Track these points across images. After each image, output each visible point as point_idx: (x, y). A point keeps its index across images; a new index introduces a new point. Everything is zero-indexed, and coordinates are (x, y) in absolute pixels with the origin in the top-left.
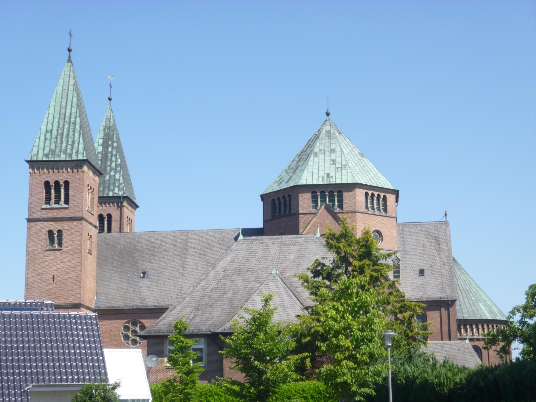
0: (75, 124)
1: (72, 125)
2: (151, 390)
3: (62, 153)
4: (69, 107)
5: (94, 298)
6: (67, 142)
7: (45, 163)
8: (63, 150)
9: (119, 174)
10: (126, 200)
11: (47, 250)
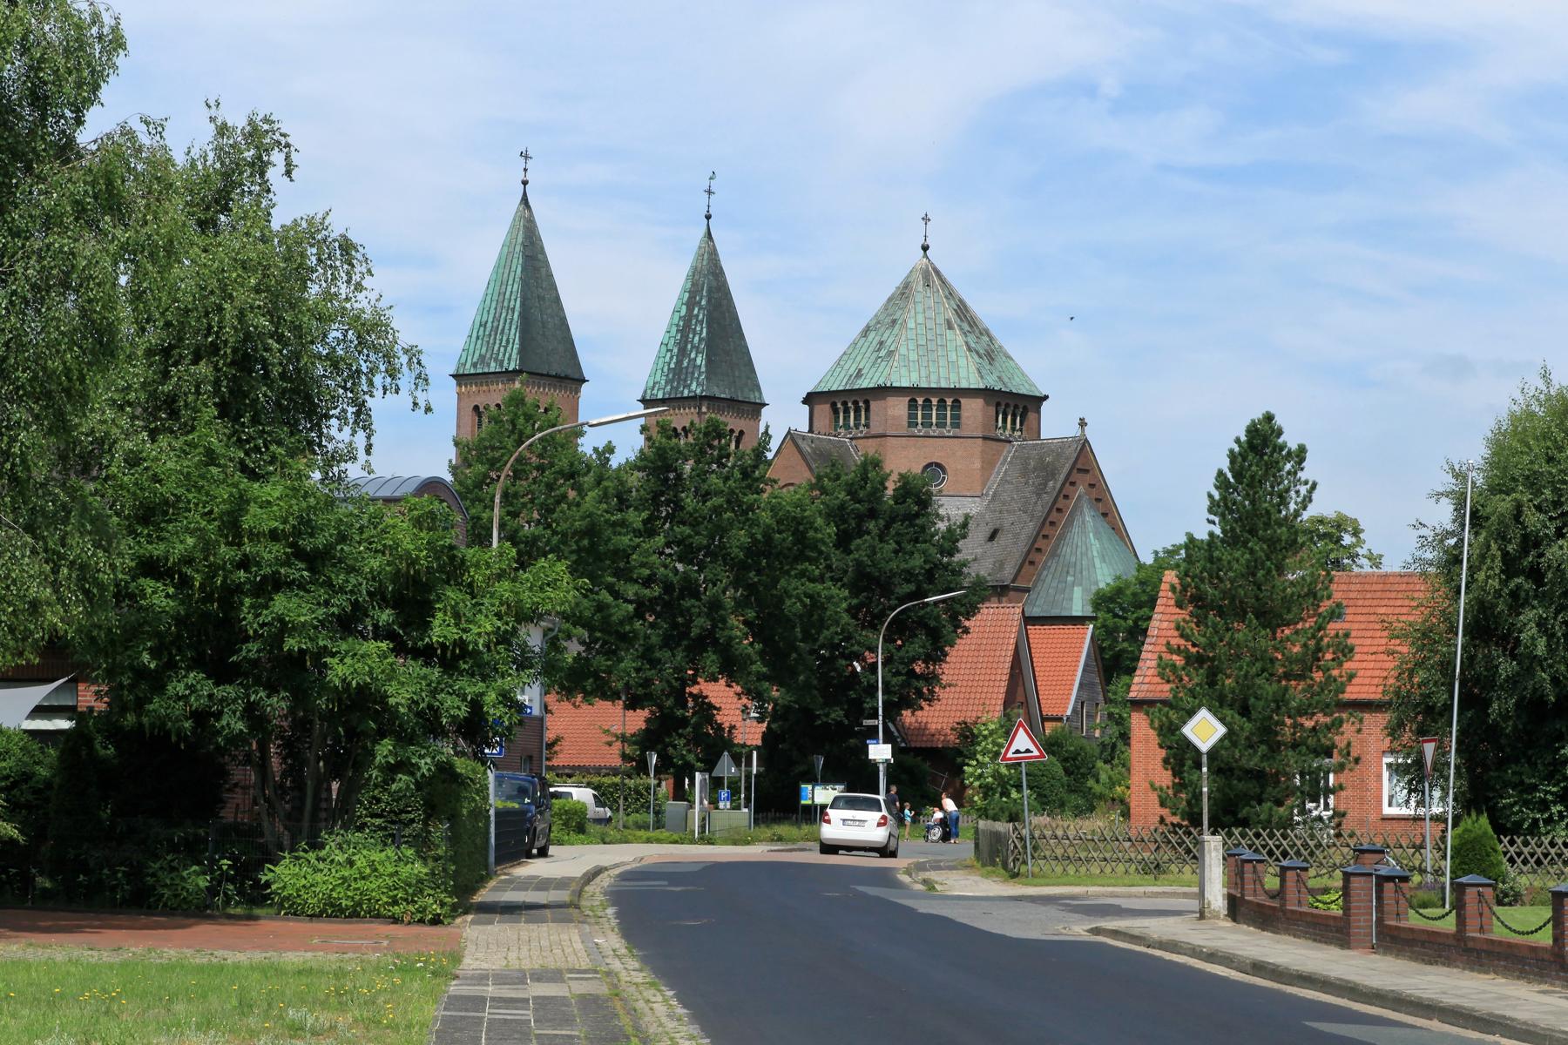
4: (510, 282)
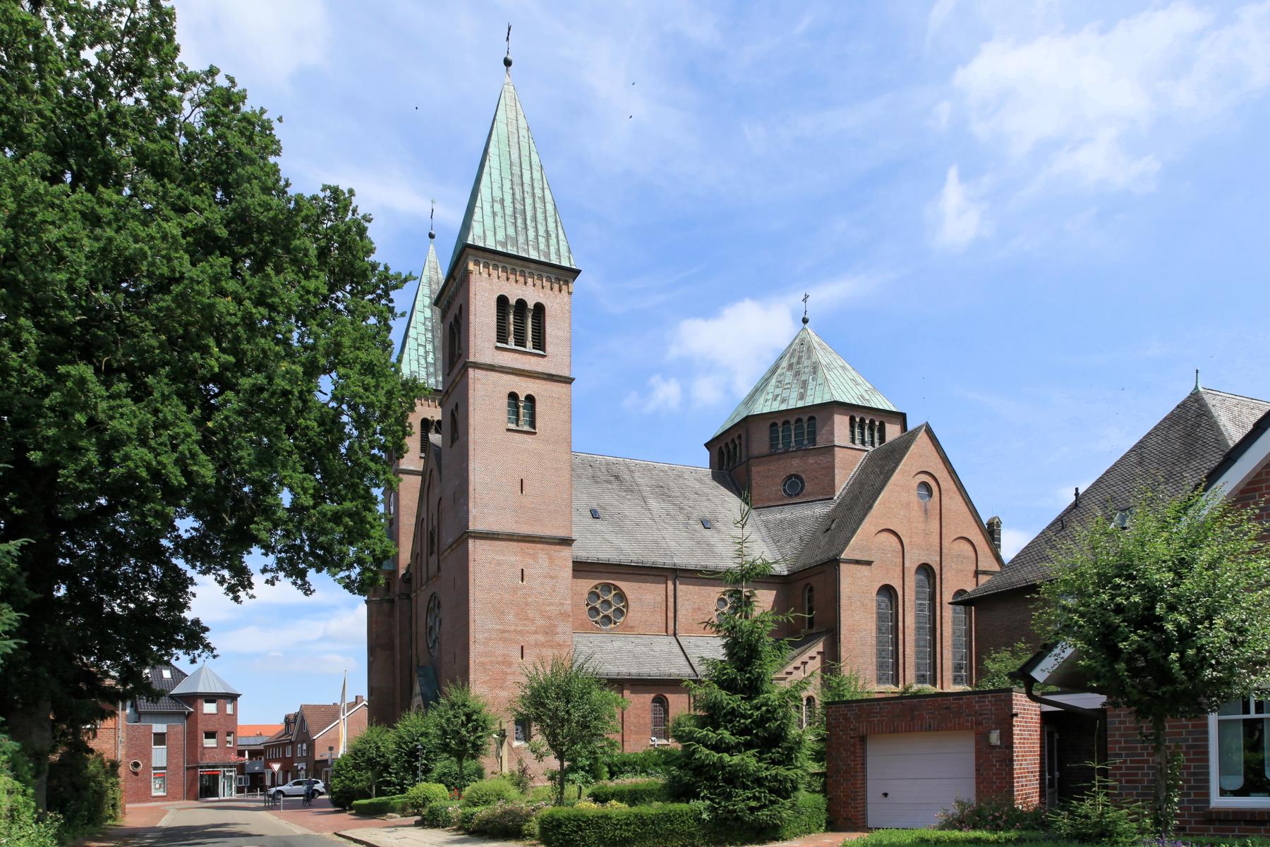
8: (531, 243)
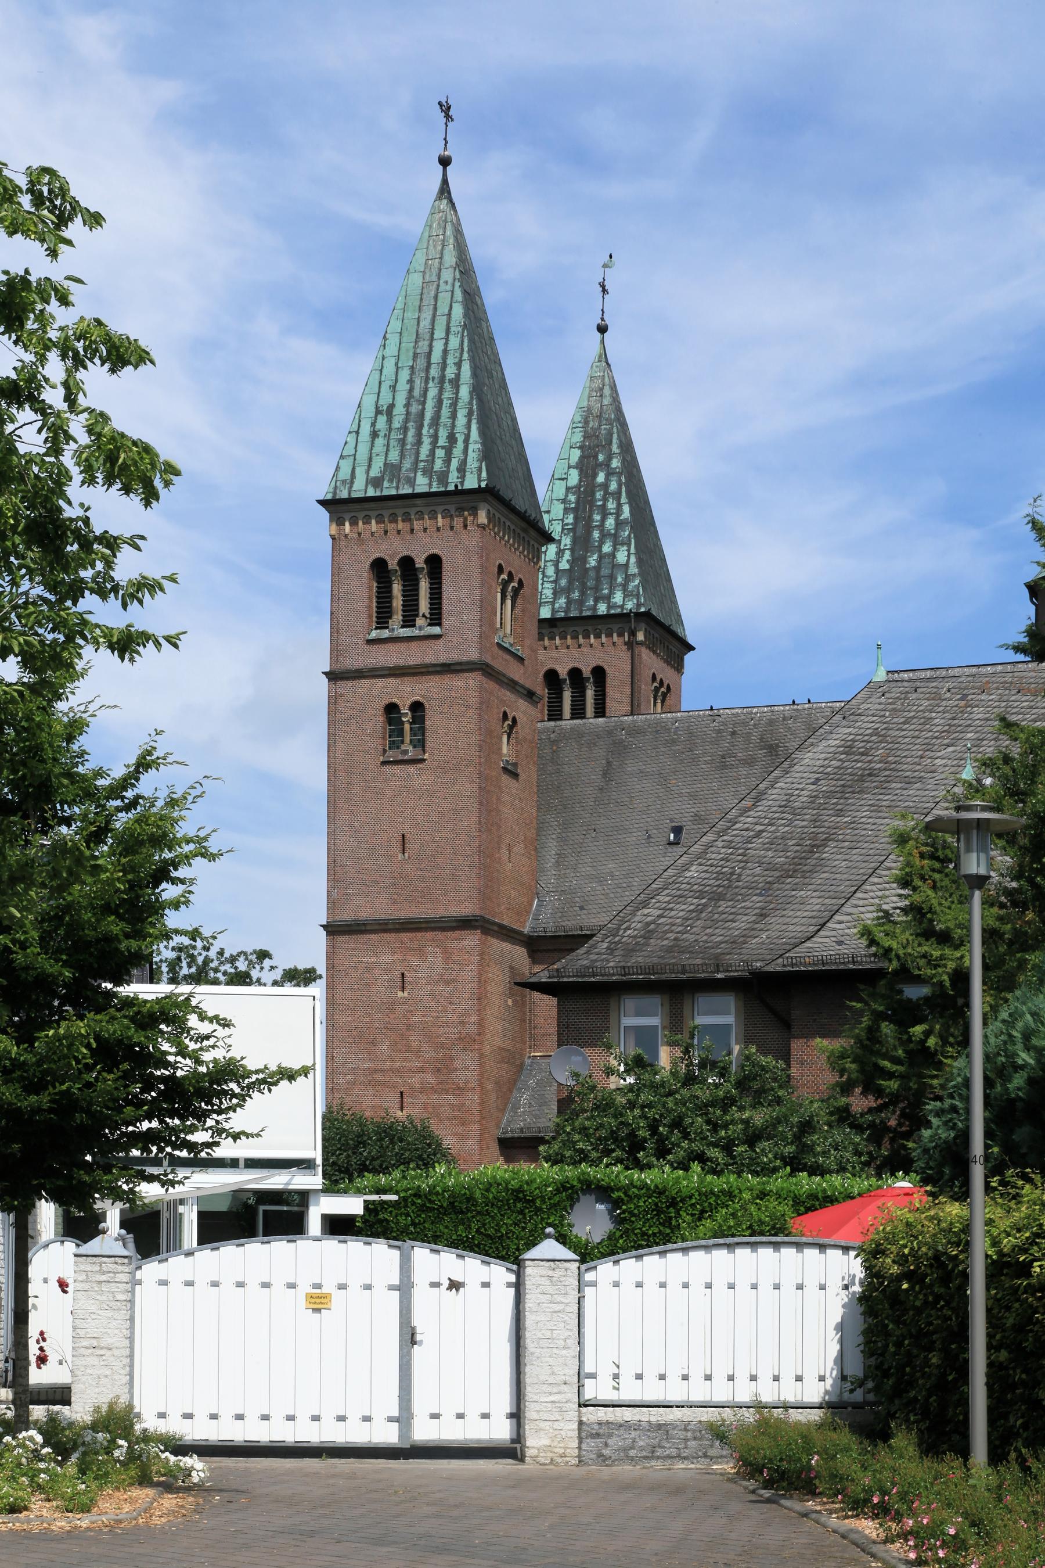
0: (456, 383)
1: (447, 386)
2: (328, 1119)
3: (419, 473)
4: (440, 333)
5: (531, 905)
6: (435, 438)
7: (373, 505)
9: (625, 548)
10: (647, 624)
11: (384, 763)
